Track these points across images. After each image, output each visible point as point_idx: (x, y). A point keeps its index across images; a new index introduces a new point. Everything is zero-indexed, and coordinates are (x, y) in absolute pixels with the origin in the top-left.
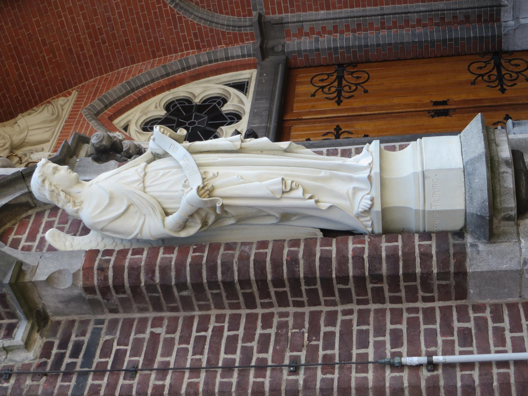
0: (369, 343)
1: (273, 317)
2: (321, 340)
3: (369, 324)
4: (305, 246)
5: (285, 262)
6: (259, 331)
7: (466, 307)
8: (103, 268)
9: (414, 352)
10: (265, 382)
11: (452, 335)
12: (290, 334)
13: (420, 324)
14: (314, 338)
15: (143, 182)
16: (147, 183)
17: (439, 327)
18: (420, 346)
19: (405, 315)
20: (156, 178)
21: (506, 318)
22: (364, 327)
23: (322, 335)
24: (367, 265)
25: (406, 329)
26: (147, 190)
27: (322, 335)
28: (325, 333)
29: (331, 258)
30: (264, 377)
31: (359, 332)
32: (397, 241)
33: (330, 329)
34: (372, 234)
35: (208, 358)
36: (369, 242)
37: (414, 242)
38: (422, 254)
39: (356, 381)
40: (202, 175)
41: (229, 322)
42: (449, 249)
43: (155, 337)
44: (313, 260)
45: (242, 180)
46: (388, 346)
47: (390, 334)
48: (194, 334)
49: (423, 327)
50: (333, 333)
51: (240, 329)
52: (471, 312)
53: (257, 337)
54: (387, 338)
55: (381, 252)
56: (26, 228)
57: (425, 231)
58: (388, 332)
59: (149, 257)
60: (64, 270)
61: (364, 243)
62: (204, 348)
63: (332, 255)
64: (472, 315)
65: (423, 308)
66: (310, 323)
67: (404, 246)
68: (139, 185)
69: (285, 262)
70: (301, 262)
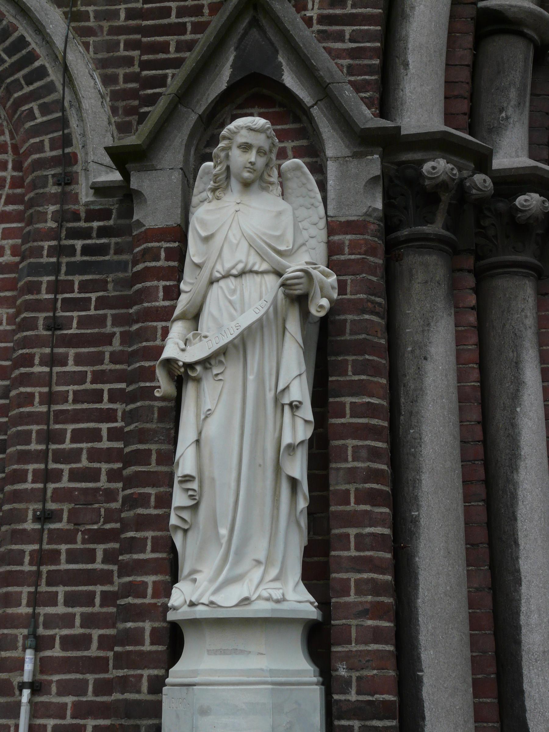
0: (72, 607)
2: (82, 546)
3: (101, 606)
4: (158, 515)
9: (19, 665)
10: (27, 483)
11: (73, 717)
12: (96, 506)
13: (96, 673)
14: (86, 537)
16: (222, 283)
17: (89, 699)
18: (59, 673)
22: (98, 600)
23: (92, 546)
25: (89, 655)
27: (92, 546)
28: (94, 550)
30: (33, 482)
31: (92, 594)
32: (152, 643)
33: (100, 556)
34: (166, 609)
35: (68, 410)
36: (155, 604)
39: (16, 592)
43: (108, 339)
45: (203, 417)
46: (66, 632)
47: (84, 635)
49: (91, 678)
50: (93, 560)
51: (109, 443)
53: (96, 465)
54: (78, 631)
58: (87, 631)
59: (157, 311)
61: (153, 597)
62: (83, 402)
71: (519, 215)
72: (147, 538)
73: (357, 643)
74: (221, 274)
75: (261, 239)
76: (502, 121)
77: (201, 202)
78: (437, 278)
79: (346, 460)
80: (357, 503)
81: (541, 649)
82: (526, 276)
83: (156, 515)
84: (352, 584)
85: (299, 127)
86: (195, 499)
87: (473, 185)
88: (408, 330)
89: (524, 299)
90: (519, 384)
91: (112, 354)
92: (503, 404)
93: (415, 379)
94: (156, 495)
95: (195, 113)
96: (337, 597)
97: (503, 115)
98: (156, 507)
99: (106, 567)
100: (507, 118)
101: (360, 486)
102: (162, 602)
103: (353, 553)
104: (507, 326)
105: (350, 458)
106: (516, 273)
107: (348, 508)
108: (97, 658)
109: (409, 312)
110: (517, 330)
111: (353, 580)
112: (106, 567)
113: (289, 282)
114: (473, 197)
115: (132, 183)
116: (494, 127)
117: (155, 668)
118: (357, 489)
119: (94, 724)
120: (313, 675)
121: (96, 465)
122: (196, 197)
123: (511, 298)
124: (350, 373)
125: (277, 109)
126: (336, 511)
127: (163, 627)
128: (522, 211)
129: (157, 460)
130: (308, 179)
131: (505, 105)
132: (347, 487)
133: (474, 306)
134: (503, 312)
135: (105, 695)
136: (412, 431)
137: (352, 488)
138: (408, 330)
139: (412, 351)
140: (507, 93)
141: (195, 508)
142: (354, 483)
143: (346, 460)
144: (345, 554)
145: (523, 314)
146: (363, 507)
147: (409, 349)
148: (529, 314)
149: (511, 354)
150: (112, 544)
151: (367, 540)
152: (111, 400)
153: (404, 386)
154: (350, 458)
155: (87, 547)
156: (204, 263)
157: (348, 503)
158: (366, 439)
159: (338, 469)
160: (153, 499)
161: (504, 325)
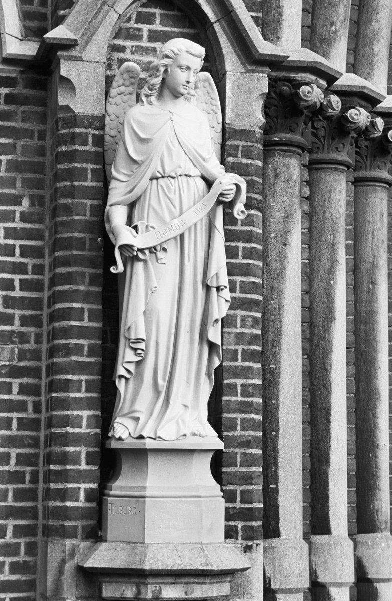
1: (36, 326)
5: (67, 341)
6: (17, 313)
7: (35, 535)
8: (75, 138)
15: (163, 177)
17: (9, 504)
19: (28, 469)
20: (166, 191)
21: (14, 577)
24: (59, 431)
26: (154, 181)
29: (68, 392)
33: (15, 389)
37: (84, 482)
38: (65, 490)
40: (160, 244)
41: (32, 279)
42: (70, 520)
44: (68, 372)
48: (18, 243)
49: (10, 487)
52: (28, 540)
53: (10, 311)
55: (72, 446)
56: (172, 27)
57: (104, 495)
60: (75, 94)
63: (72, 392)
64: (22, 541)
65: (37, 489)
66: (25, 367)
67: (79, 471)
68: (158, 172)
69: (67, 341)
70: (67, 359)
71: (349, 125)
72: (82, 381)
73: (240, 466)
74: (161, 174)
75: (194, 149)
76: (332, 34)
77: (119, 94)
78: (295, 178)
79: (236, 326)
80: (243, 360)
81: (337, 467)
82: (342, 171)
83: (88, 362)
84: (239, 422)
85: (194, 32)
86: (141, 356)
87: (329, 104)
88: (271, 220)
89: (340, 191)
90: (334, 262)
91: (22, 213)
92: (321, 276)
93: (276, 261)
94: (89, 346)
95: (116, 12)
96: (228, 431)
97: (333, 28)
98: (88, 356)
99: (21, 398)
100: (336, 31)
101: (246, 347)
102: (94, 431)
103: (240, 399)
104: (327, 213)
105: (239, 325)
106: (337, 169)
107: (236, 364)
108: (16, 472)
109: (274, 204)
110: (334, 217)
111: (239, 419)
112: (21, 398)
113: (225, 192)
114: (328, 114)
115: (61, 70)
116: (325, 38)
117: (90, 482)
118: (243, 350)
119: (14, 524)
120: (254, 493)
121: (10, 311)
122: (115, 90)
123: (331, 190)
124: (240, 257)
125: (175, 13)
126: (227, 366)
127: (96, 451)
128: (352, 123)
129: (89, 317)
130: (212, 89)
131: (335, 20)
132: (236, 347)
133: (308, 197)
134: (325, 201)
135: (22, 501)
136: (272, 302)
137: (240, 348)
138: (271, 220)
139: (275, 238)
140: (337, 8)
141: (139, 364)
142: (241, 344)
143: (236, 326)
144: (234, 399)
145: (339, 204)
146: (247, 364)
147: (273, 235)
148: (342, 204)
149: (329, 236)
150: (26, 378)
151: (250, 389)
152: (22, 255)
153: (267, 265)
154: (239, 325)
155: (4, 380)
156: (143, 162)
157: (237, 360)
158: (251, 311)
159: (229, 333)
160: (86, 349)
161: (325, 212)
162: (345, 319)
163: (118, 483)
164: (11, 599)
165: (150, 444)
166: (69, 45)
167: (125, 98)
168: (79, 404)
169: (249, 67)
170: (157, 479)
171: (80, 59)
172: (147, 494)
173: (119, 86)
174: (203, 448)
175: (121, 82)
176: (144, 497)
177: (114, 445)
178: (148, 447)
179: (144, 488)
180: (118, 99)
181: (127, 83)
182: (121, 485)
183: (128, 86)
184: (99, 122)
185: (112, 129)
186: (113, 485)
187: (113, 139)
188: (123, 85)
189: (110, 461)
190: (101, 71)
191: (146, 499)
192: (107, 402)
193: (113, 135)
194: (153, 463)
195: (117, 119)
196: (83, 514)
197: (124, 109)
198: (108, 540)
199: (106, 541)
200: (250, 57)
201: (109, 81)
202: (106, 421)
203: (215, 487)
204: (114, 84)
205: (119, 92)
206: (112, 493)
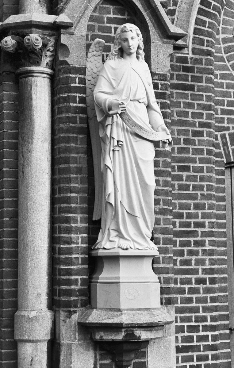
77: (92, 56)
122: (90, 53)
162: (19, 257)
163: (101, 276)
164: (190, 366)
165: (122, 253)
166: (67, 26)
167: (96, 58)
168: (78, 231)
169: (165, 40)
170: (125, 272)
171: (73, 33)
172: (121, 281)
173: (93, 52)
174: (150, 255)
175: (94, 49)
176: (119, 283)
177: (101, 252)
178: (120, 255)
179: (119, 278)
180: (92, 59)
181: (98, 49)
182: (106, 275)
183: (98, 52)
184: (82, 71)
185: (89, 76)
186: (100, 276)
187: (89, 81)
188: (95, 51)
189: (95, 263)
190: (84, 42)
191: (121, 284)
192: (94, 228)
193: (89, 79)
194: (123, 264)
195: (92, 70)
196: (81, 293)
197: (96, 64)
198: (98, 306)
199: (96, 308)
200: (166, 34)
201: (88, 46)
202: (92, 240)
203: (154, 277)
204: (90, 50)
205: (93, 55)
206: (99, 281)
